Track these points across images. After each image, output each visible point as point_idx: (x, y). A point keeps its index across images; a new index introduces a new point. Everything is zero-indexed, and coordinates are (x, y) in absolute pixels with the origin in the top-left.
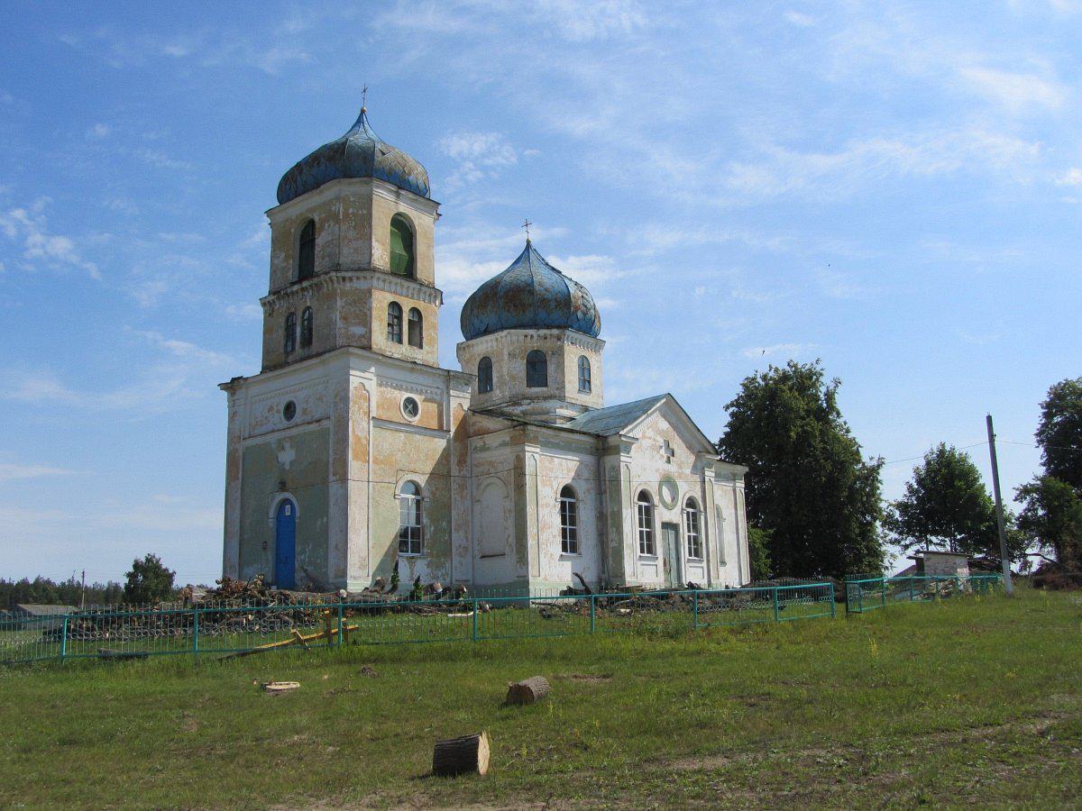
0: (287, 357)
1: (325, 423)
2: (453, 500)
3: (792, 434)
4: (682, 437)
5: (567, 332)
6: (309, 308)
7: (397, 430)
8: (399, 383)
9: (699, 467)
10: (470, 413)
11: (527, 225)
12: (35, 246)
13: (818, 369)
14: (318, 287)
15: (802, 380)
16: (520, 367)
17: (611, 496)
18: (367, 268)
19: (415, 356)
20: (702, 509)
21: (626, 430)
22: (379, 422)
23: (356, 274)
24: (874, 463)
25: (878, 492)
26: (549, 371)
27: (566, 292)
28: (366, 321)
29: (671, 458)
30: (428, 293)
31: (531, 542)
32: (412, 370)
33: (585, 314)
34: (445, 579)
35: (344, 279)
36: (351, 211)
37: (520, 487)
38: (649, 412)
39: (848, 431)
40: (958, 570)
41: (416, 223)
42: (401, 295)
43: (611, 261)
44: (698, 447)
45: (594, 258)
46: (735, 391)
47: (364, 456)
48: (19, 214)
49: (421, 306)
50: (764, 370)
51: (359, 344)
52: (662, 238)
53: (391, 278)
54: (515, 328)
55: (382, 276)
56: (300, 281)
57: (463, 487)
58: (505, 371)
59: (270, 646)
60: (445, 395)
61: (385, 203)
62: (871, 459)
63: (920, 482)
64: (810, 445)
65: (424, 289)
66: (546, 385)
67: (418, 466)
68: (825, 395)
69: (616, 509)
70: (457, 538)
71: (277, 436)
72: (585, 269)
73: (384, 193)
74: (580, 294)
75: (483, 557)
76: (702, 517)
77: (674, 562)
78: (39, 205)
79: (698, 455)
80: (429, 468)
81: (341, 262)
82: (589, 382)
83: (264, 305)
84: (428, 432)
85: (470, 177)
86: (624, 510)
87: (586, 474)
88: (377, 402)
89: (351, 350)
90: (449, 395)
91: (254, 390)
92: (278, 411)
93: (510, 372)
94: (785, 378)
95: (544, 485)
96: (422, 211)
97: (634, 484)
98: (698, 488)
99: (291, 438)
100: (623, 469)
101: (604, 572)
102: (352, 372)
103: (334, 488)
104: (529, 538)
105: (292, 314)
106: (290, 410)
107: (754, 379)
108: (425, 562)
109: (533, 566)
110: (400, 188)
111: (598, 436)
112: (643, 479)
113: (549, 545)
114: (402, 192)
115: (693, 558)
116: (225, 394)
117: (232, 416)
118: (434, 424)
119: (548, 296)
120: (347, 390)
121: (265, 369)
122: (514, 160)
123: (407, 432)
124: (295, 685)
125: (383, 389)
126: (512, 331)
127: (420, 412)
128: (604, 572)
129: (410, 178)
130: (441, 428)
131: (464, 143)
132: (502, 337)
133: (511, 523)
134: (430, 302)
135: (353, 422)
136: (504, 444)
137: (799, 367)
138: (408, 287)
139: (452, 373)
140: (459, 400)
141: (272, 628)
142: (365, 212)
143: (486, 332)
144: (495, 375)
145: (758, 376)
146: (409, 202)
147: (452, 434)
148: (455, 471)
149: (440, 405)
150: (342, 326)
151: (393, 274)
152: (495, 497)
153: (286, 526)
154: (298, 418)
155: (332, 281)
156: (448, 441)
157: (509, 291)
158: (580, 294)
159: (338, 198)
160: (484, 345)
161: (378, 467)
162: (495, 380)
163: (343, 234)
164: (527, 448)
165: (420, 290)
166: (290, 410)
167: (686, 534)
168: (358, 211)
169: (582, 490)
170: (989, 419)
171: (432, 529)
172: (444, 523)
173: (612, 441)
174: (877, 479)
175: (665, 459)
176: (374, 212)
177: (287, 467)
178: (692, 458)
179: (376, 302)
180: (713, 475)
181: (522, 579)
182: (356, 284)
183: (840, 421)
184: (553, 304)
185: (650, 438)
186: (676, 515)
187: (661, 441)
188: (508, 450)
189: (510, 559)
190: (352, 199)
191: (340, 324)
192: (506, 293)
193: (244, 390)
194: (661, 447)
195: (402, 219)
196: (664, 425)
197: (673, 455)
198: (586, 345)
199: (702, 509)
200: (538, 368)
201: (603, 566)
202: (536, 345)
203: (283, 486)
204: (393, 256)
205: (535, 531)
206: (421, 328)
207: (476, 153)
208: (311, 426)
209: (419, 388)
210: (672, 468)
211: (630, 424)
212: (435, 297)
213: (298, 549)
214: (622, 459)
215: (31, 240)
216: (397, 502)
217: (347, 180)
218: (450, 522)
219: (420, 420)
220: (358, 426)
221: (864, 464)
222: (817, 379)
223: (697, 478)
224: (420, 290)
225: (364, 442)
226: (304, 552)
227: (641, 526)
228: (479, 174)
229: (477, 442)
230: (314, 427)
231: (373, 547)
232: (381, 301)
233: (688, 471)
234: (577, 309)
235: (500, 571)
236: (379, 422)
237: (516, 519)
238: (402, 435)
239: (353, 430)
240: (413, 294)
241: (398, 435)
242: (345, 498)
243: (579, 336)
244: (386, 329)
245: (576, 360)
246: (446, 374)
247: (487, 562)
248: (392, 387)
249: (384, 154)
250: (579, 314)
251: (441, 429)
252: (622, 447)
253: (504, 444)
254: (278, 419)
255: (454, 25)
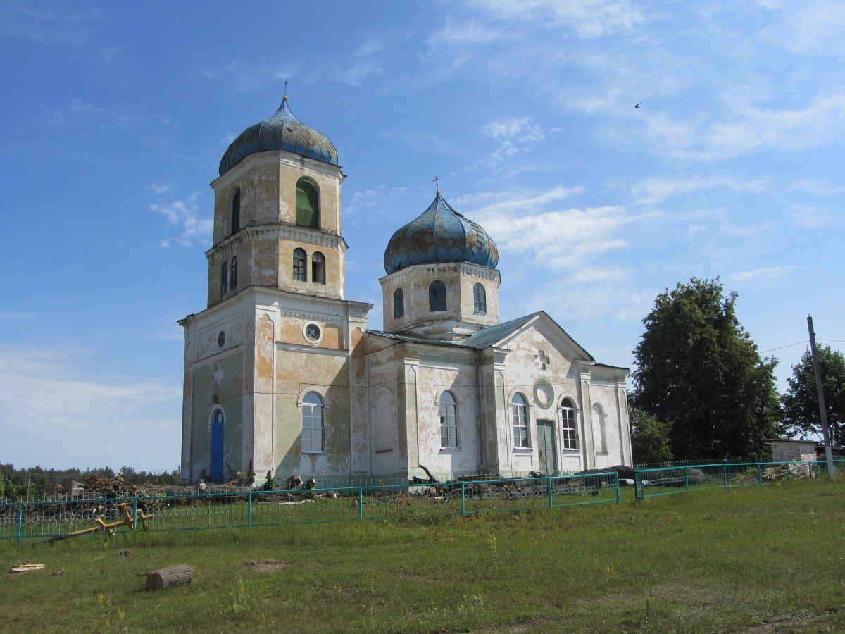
0: (222, 297)
1: (241, 347)
2: (351, 407)
3: (690, 340)
4: (555, 344)
5: (462, 265)
6: (235, 257)
7: (299, 351)
8: (302, 313)
9: (575, 370)
10: (367, 335)
11: (436, 180)
12: (190, 228)
13: (718, 284)
14: (240, 239)
15: (703, 296)
16: (424, 296)
17: (487, 399)
18: (275, 223)
19: (319, 290)
20: (578, 407)
21: (498, 344)
22: (282, 345)
23: (268, 227)
24: (768, 362)
25: (774, 387)
26: (448, 298)
27: (462, 232)
28: (274, 265)
29: (547, 365)
30: (330, 239)
31: (410, 439)
32: (313, 302)
33: (480, 249)
34: (344, 471)
35: (257, 232)
36: (263, 178)
37: (401, 394)
38: (522, 327)
39: (747, 336)
40: (802, 456)
41: (320, 183)
42: (306, 242)
43: (622, 209)
44: (574, 355)
45: (608, 208)
46: (650, 307)
47: (268, 372)
48: (179, 204)
49: (324, 250)
50: (673, 288)
51: (269, 284)
52: (659, 188)
53: (295, 229)
54: (420, 263)
55: (287, 229)
56: (233, 234)
57: (360, 396)
58: (412, 299)
59: (89, 530)
60: (345, 320)
61: (291, 170)
62: (766, 359)
63: (801, 377)
64: (708, 349)
65: (326, 236)
66: (445, 309)
67: (320, 380)
68: (724, 306)
69: (491, 410)
70: (356, 437)
71: (213, 359)
72: (601, 217)
73: (291, 162)
74: (475, 233)
75: (377, 452)
76: (579, 415)
77: (550, 453)
78: (193, 198)
79: (574, 362)
80: (330, 380)
81: (256, 219)
82: (485, 305)
83: (208, 257)
84: (328, 351)
85: (509, 152)
86: (497, 411)
87: (465, 381)
88: (282, 329)
89: (255, 288)
90: (348, 321)
91: (200, 324)
92: (215, 340)
93: (417, 299)
94: (689, 293)
95: (423, 391)
96: (326, 174)
97: (509, 388)
98: (574, 390)
99: (221, 361)
100: (496, 376)
101: (482, 463)
102: (257, 306)
103: (245, 399)
104: (408, 436)
105: (226, 263)
106: (221, 339)
107: (665, 296)
108: (326, 457)
109: (412, 460)
110: (304, 157)
111: (475, 349)
112: (517, 383)
113: (428, 441)
114: (306, 160)
115: (570, 449)
116: (182, 328)
117: (188, 345)
118: (335, 345)
119: (446, 235)
120: (253, 321)
121: (209, 307)
122: (542, 136)
123: (308, 352)
124: (39, 567)
125: (288, 318)
126: (417, 266)
127: (321, 335)
128: (482, 463)
129: (315, 148)
130: (341, 348)
131: (503, 126)
132: (409, 272)
133: (396, 424)
134: (332, 247)
135: (259, 346)
136: (390, 359)
137: (701, 284)
138: (312, 236)
139: (349, 303)
140: (357, 325)
141: (113, 516)
142: (274, 178)
143: (400, 268)
144: (405, 303)
145: (669, 293)
146: (313, 168)
147: (350, 352)
148: (353, 382)
149: (340, 330)
150: (255, 269)
151: (298, 225)
152: (385, 402)
153: (218, 429)
154: (226, 344)
155: (248, 235)
156: (347, 358)
157: (416, 233)
158: (475, 233)
159: (254, 169)
160: (399, 278)
161: (281, 381)
162: (405, 307)
163: (257, 197)
164: (406, 362)
165: (322, 237)
166: (221, 339)
167: (562, 429)
168: (269, 178)
169: (461, 393)
170: (810, 320)
171: (333, 430)
172: (344, 426)
173: (487, 352)
174: (771, 377)
175: (541, 365)
176: (281, 178)
177: (219, 384)
178: (568, 365)
179: (282, 249)
180: (589, 378)
181: (403, 470)
182: (267, 236)
183: (738, 327)
184: (451, 243)
185: (525, 349)
186: (552, 414)
187: (536, 351)
188: (392, 364)
189: (396, 454)
190: (264, 169)
191: (254, 268)
192: (413, 236)
193: (194, 324)
194: (536, 356)
195: (308, 181)
196: (539, 337)
197: (549, 363)
198: (480, 274)
199: (578, 407)
200: (439, 295)
201: (482, 458)
202: (436, 276)
203: (216, 399)
204: (299, 212)
205: (414, 430)
206: (324, 268)
207: (513, 134)
208: (233, 350)
209: (320, 316)
210: (548, 374)
211: (502, 338)
212: (337, 242)
213: (225, 449)
214: (495, 367)
215: (187, 223)
216: (300, 409)
217: (261, 154)
218: (348, 425)
219: (322, 342)
220: (263, 349)
221: (762, 364)
222: (717, 294)
223: (573, 381)
224: (322, 237)
225: (269, 362)
226: (228, 451)
227: (565, 426)
228: (515, 149)
229: (372, 358)
230: (234, 351)
231: (277, 446)
232: (286, 249)
233: (564, 376)
234: (472, 245)
235: (388, 464)
236: (282, 345)
237: (399, 420)
238: (304, 354)
239: (259, 352)
240: (316, 241)
241: (299, 355)
242: (252, 407)
243: (477, 267)
244: (291, 270)
245: (471, 287)
246: (344, 304)
247: (381, 456)
248: (295, 316)
249: (290, 131)
250: (475, 250)
251: (342, 349)
252: (495, 358)
253: (390, 359)
254: (215, 345)
255: (490, 36)
